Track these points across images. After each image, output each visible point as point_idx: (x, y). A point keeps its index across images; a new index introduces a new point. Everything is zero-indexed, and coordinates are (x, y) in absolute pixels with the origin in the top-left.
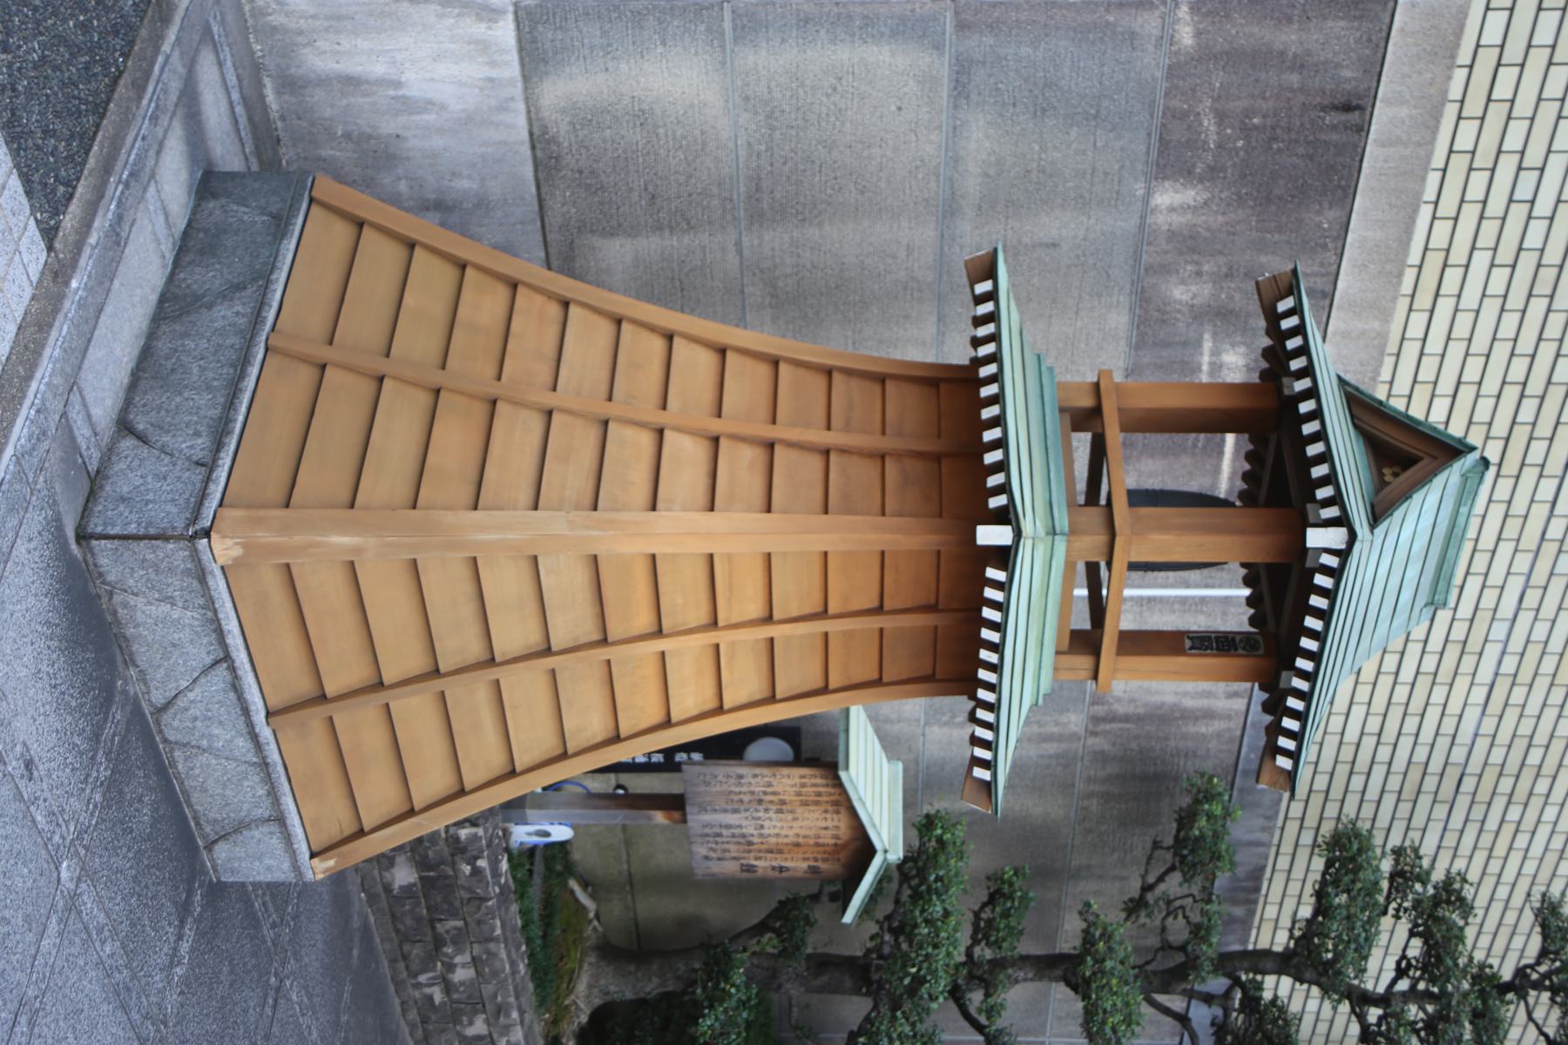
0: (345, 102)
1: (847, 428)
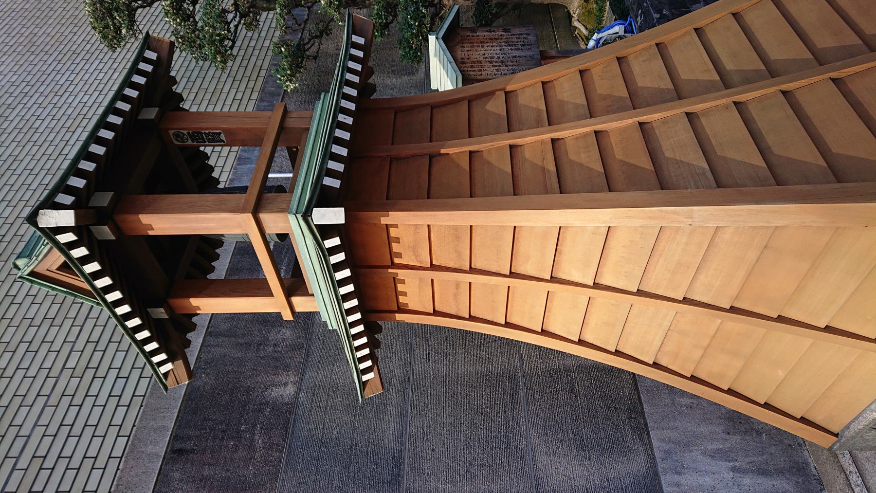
0: (765, 457)
1: (458, 285)
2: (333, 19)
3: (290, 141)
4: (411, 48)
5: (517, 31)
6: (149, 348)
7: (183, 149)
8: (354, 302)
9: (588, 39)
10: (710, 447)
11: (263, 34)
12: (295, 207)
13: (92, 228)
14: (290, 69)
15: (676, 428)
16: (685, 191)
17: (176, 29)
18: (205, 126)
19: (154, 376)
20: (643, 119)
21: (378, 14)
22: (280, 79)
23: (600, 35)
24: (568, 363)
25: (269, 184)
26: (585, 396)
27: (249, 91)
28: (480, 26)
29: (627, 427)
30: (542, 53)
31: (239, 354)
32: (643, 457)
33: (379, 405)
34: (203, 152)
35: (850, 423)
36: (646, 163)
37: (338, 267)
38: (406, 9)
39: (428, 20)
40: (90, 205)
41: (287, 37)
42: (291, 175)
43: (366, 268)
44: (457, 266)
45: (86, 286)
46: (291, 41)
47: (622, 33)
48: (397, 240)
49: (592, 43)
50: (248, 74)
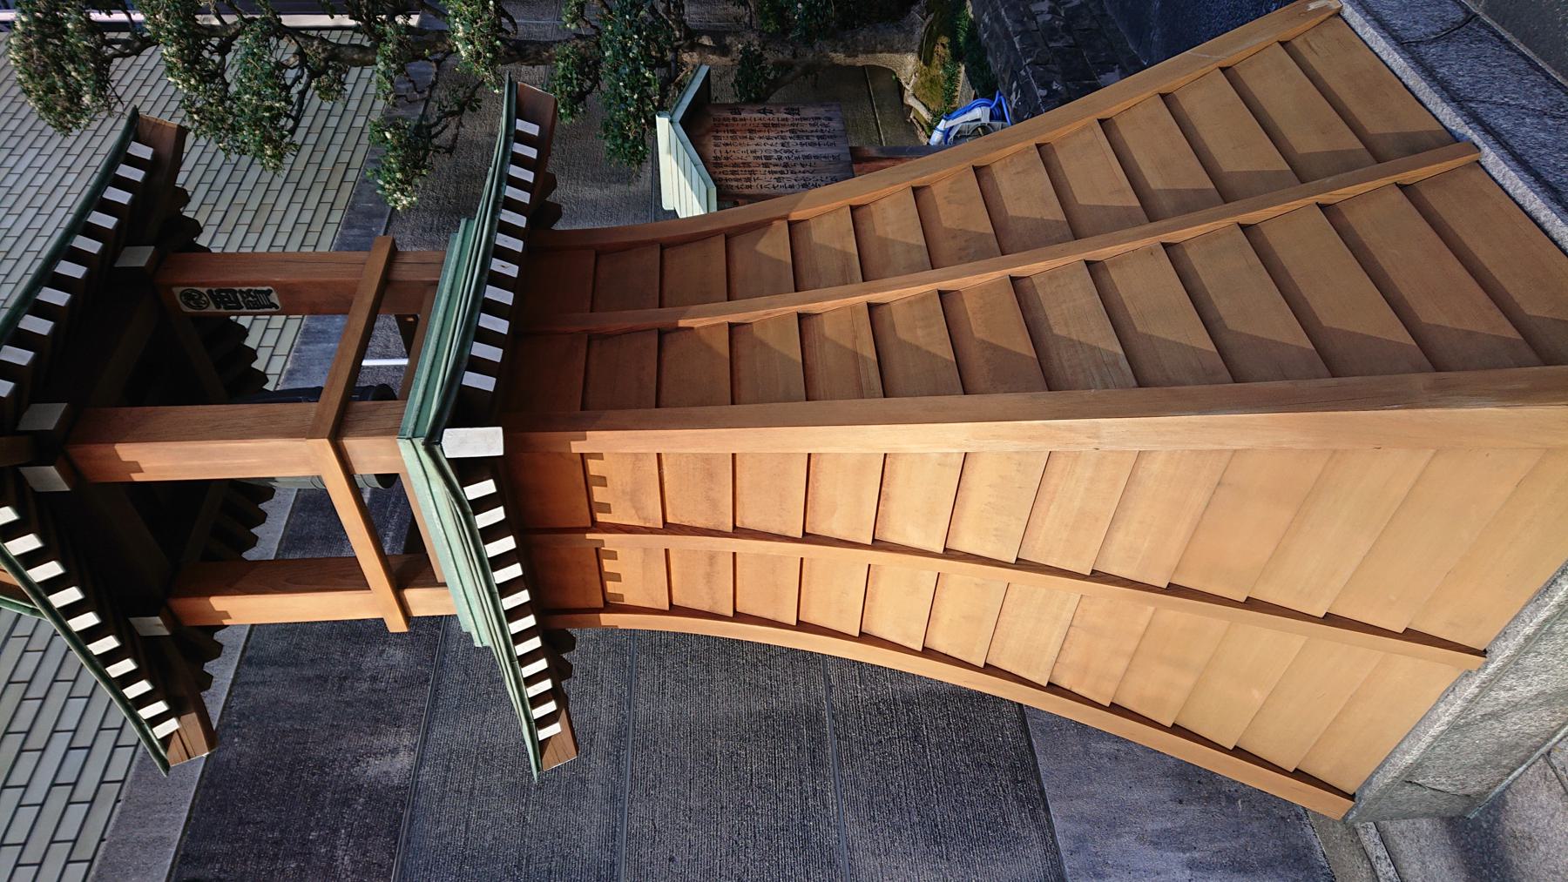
0: (1242, 841)
1: (712, 558)
2: (482, 83)
3: (400, 300)
4: (625, 138)
5: (809, 112)
6: (132, 692)
7: (198, 320)
8: (523, 597)
9: (932, 128)
10: (1150, 827)
11: (353, 105)
12: (411, 426)
13: (25, 471)
14: (402, 170)
15: (1093, 796)
16: (1086, 392)
17: (187, 97)
18: (241, 279)
19: (143, 743)
20: (1018, 271)
21: (564, 77)
22: (383, 188)
23: (951, 123)
24: (910, 688)
25: (365, 381)
26: (939, 745)
27: (325, 208)
28: (746, 103)
29: (1010, 799)
30: (853, 150)
31: (305, 698)
32: (1038, 849)
33: (570, 784)
34: (235, 323)
35: (1372, 776)
36: (1021, 345)
37: (491, 533)
38: (616, 71)
39: (654, 89)
40: (22, 427)
41: (400, 112)
42: (405, 362)
43: (545, 534)
44: (710, 525)
45: (11, 579)
46: (405, 120)
47: (986, 120)
48: (603, 481)
49: (936, 137)
50: (323, 177)
